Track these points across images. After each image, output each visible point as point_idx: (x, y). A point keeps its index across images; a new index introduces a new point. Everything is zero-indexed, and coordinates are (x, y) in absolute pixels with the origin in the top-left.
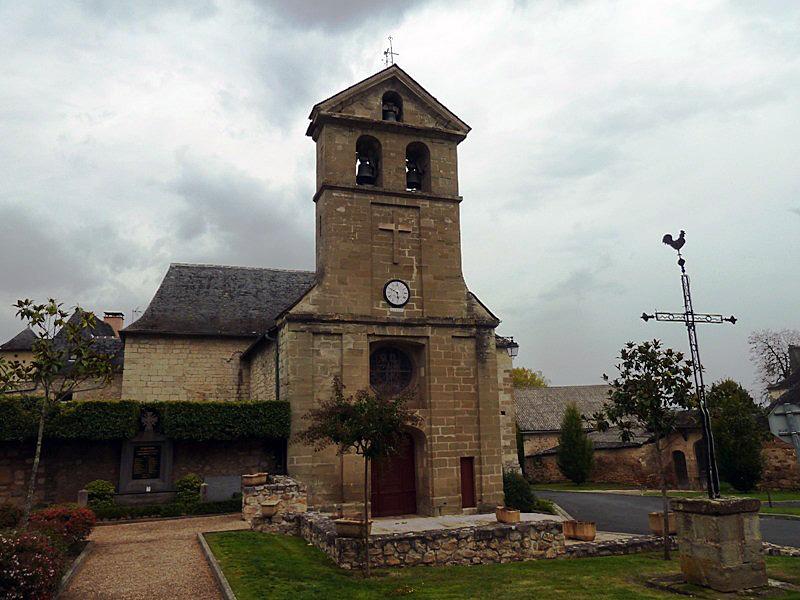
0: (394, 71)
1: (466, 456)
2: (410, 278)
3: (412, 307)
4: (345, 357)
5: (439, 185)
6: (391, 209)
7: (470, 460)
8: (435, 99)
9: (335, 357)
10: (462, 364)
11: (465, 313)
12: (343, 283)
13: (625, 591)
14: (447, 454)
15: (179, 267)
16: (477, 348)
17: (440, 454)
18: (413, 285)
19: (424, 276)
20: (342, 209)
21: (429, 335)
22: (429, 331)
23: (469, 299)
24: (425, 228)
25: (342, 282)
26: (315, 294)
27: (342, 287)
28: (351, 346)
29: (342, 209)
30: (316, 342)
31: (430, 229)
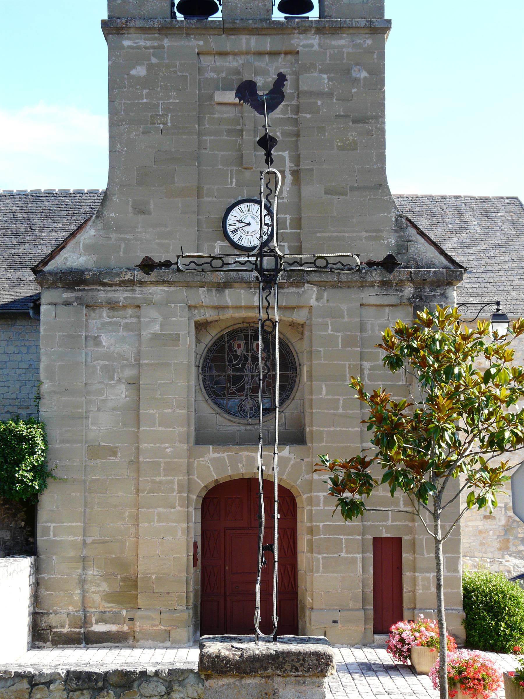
4: (144, 349)
7: (396, 543)
9: (127, 349)
12: (142, 212)
19: (303, 188)
20: (140, 71)
21: (313, 302)
23: (399, 228)
24: (310, 94)
25: (141, 210)
26: (90, 233)
27: (141, 218)
28: (157, 328)
29: (140, 71)
31: (320, 94)
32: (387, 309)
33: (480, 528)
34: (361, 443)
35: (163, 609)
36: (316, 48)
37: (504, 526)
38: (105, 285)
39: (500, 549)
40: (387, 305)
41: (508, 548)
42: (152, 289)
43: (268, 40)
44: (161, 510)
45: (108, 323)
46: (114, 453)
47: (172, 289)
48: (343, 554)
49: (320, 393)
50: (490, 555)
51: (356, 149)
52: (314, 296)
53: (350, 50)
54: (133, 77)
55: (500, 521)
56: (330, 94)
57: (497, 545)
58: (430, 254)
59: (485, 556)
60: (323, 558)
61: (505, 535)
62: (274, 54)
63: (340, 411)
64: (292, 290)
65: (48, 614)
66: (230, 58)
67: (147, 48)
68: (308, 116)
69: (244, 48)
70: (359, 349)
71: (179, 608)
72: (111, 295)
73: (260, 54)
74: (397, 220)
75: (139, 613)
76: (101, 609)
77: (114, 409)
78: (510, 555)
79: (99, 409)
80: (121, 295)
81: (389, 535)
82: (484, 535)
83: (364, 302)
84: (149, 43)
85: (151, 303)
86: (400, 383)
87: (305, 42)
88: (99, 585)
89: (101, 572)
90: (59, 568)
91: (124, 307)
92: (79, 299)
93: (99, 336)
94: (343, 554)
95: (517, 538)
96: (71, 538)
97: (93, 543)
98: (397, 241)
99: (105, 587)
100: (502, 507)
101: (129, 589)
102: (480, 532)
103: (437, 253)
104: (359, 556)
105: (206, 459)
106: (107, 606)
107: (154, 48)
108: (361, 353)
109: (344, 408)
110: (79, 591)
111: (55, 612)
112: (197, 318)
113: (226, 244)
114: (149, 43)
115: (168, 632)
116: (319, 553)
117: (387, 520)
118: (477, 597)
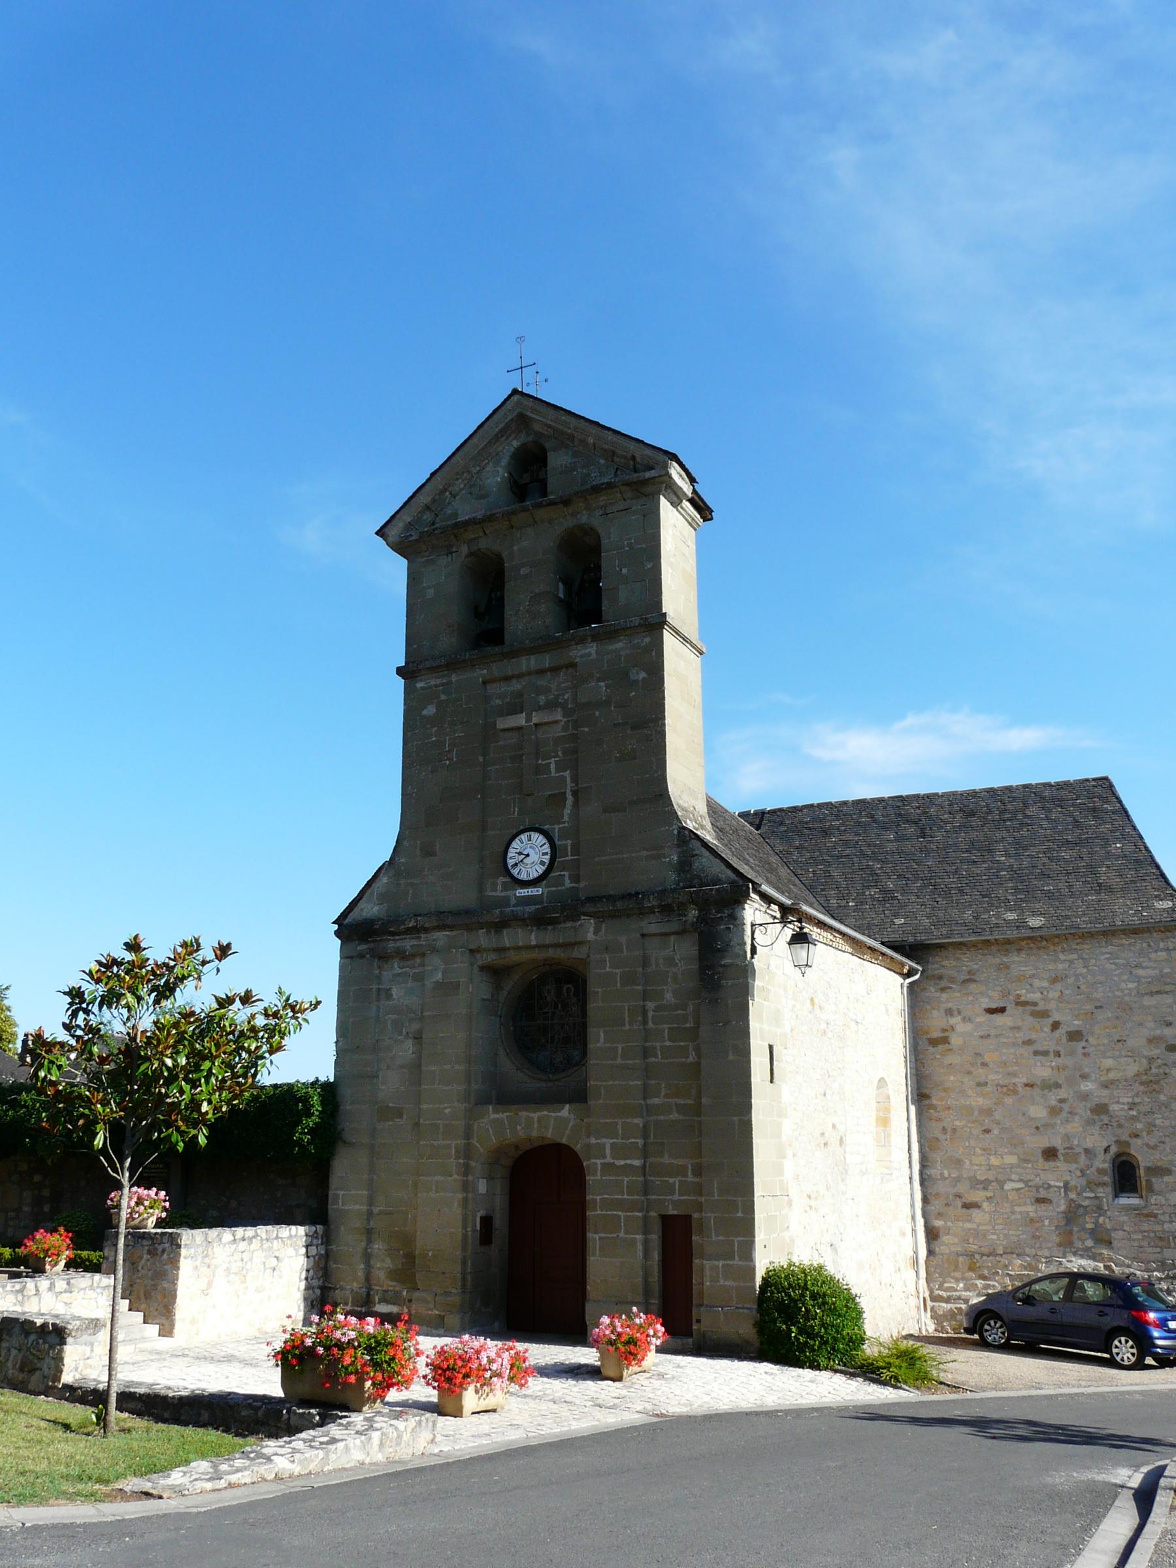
0: (518, 403)
1: (672, 1212)
2: (558, 819)
3: (560, 881)
5: (618, 597)
6: (524, 682)
8: (597, 424)
10: (669, 996)
11: (673, 877)
13: (442, 1352)
14: (620, 1205)
15: (1111, 786)
16: (702, 957)
17: (606, 1204)
18: (564, 834)
20: (430, 710)
21: (590, 936)
22: (589, 930)
25: (428, 852)
29: (430, 710)
30: (385, 973)
32: (672, 938)
33: (1032, 1214)
34: (645, 1099)
35: (439, 1291)
36: (594, 656)
37: (1065, 1212)
38: (393, 934)
39: (1059, 1245)
40: (673, 933)
41: (1070, 1244)
42: (437, 935)
43: (547, 656)
44: (439, 1178)
45: (399, 975)
46: (401, 1116)
47: (454, 933)
48: (622, 1235)
49: (598, 1041)
50: (1047, 1253)
51: (635, 758)
52: (592, 929)
53: (628, 652)
54: (425, 717)
55: (1058, 1206)
56: (608, 703)
57: (1056, 1239)
58: (717, 868)
59: (1039, 1253)
60: (600, 1238)
61: (1066, 1225)
62: (555, 670)
63: (619, 1061)
64: (569, 924)
65: (335, 1289)
66: (514, 681)
67: (436, 686)
68: (586, 729)
69: (524, 668)
70: (640, 988)
71: (454, 1291)
72: (399, 944)
73: (541, 672)
74: (679, 833)
75: (416, 1294)
76: (385, 1288)
77: (402, 1067)
78: (1075, 1254)
79: (388, 1067)
80: (408, 944)
81: (676, 1212)
82: (1037, 1225)
83: (645, 931)
84: (438, 681)
85: (434, 950)
86: (688, 1025)
87: (583, 652)
88: (383, 1261)
89: (386, 1247)
90: (349, 1241)
91: (413, 956)
92: (371, 950)
93: (389, 989)
94: (622, 1235)
95: (1084, 1229)
96: (357, 1207)
97: (378, 1214)
98: (679, 857)
99: (388, 1263)
100: (1059, 1187)
101: (408, 1269)
102: (1032, 1220)
103: (723, 867)
104: (639, 1237)
105: (485, 1120)
106: (391, 1285)
107: (443, 684)
108: (644, 991)
109: (623, 1057)
110: (362, 1266)
111: (342, 1289)
112: (480, 963)
113: (508, 879)
114: (438, 681)
115: (442, 1318)
116: (596, 1232)
117: (673, 1193)
118: (772, 1293)
